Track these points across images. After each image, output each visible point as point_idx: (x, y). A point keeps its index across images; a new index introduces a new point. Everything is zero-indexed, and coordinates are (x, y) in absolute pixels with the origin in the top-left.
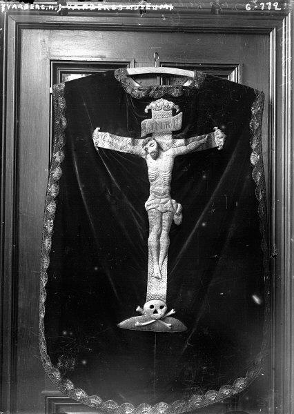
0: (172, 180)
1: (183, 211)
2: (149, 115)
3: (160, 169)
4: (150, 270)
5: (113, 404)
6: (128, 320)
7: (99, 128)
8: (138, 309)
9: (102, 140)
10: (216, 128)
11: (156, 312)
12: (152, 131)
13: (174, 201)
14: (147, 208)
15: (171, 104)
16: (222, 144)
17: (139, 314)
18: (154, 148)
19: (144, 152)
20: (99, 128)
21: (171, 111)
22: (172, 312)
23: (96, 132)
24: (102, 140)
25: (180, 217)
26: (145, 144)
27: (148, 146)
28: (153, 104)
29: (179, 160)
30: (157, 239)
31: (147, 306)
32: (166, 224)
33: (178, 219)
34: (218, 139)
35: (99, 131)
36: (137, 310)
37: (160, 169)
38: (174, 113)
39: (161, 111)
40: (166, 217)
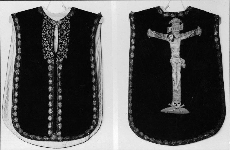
0: (93, 116)
1: (186, 63)
2: (171, 25)
3: (175, 47)
4: (174, 88)
5: (159, 141)
6: (165, 109)
7: (150, 29)
8: (169, 104)
9: (151, 34)
10: (198, 27)
11: (176, 105)
12: (171, 31)
13: (182, 59)
14: (171, 62)
15: (180, 21)
16: (201, 33)
17: (170, 106)
18: (172, 38)
19: (168, 39)
20: (150, 29)
21: (179, 23)
22: (183, 105)
23: (149, 30)
24: (151, 34)
25: (185, 64)
26: (168, 36)
27: (170, 37)
28: (172, 21)
29: (183, 42)
30: (177, 76)
31: (173, 103)
32: (179, 69)
33: (184, 66)
34: (199, 31)
35: (150, 30)
36: (169, 105)
37: (175, 47)
38: (180, 24)
39: (176, 26)
40: (179, 64)
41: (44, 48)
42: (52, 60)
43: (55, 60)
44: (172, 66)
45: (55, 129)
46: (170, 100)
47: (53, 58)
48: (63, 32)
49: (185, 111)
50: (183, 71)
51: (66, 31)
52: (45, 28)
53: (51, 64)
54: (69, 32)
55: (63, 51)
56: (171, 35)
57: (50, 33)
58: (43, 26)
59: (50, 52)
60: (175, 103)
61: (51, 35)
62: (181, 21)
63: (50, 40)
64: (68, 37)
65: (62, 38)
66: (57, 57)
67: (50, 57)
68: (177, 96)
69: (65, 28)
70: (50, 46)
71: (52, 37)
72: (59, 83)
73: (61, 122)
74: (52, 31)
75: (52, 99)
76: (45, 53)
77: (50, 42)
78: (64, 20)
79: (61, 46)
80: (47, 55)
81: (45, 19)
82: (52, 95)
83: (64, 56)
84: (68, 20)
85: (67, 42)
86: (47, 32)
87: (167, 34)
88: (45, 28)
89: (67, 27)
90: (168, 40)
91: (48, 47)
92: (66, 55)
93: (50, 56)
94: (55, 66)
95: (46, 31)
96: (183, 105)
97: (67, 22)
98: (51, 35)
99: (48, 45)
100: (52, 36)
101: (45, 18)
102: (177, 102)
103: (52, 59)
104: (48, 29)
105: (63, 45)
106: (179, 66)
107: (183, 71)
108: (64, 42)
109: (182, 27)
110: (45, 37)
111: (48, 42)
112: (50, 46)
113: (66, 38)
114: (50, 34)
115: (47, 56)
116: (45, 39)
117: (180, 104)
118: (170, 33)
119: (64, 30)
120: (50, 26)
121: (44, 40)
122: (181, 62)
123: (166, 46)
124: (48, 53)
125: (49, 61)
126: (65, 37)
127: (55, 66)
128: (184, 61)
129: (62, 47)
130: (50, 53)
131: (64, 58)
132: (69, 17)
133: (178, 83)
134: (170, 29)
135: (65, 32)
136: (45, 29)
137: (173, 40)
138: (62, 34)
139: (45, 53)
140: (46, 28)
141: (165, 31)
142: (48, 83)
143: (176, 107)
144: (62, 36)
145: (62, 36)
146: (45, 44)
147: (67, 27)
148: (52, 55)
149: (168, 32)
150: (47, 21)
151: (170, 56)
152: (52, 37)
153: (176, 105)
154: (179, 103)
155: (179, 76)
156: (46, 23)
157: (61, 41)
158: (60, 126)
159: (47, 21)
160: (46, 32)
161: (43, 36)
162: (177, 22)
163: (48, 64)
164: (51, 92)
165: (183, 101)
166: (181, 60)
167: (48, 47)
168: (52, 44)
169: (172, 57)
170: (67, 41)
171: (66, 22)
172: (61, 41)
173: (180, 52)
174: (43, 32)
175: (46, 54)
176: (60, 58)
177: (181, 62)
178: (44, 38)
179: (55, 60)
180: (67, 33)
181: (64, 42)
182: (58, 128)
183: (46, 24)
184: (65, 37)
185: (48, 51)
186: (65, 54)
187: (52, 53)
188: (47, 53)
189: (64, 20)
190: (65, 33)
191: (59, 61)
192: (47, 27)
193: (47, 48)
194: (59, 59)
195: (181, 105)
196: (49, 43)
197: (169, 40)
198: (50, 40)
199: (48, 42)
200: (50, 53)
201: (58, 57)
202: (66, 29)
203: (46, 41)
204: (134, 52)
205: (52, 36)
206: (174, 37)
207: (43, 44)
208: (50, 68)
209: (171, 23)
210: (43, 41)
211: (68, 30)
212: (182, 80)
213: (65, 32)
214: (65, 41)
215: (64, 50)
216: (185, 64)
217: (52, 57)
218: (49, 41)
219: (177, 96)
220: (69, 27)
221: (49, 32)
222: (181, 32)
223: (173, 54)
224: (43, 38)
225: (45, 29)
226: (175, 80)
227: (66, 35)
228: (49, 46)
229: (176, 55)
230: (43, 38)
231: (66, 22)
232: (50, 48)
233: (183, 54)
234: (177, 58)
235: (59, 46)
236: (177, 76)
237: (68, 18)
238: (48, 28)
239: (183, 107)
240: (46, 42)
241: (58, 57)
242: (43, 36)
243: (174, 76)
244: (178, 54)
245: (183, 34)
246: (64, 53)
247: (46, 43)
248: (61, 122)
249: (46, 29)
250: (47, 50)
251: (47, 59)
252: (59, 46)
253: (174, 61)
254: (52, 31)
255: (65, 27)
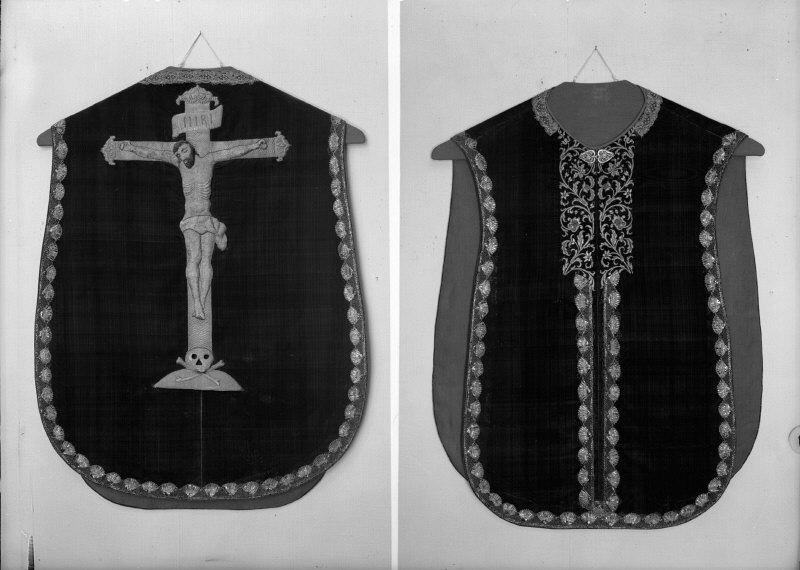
1: (227, 233)
2: (181, 109)
3: (196, 184)
4: (191, 309)
8: (179, 360)
11: (199, 363)
13: (215, 220)
15: (209, 95)
17: (181, 367)
21: (208, 105)
22: (221, 363)
25: (225, 239)
30: (199, 275)
31: (189, 357)
32: (208, 250)
33: (222, 244)
37: (196, 184)
38: (212, 106)
39: (197, 117)
40: (207, 238)
41: (568, 238)
42: (587, 277)
43: (597, 279)
44: (187, 241)
45: (599, 490)
46: (181, 345)
47: (591, 270)
48: (614, 186)
49: (223, 382)
50: (219, 260)
51: (622, 183)
52: (567, 175)
53: (585, 291)
54: (630, 187)
55: (617, 249)
56: (184, 146)
57: (585, 191)
58: (562, 168)
59: (584, 251)
60: (194, 356)
61: (588, 195)
62: (216, 100)
63: (586, 213)
64: (628, 200)
65: (612, 204)
66: (603, 269)
67: (583, 267)
68: (200, 333)
69: (617, 173)
70: (587, 231)
71: (590, 203)
72: (583, 343)
73: (618, 468)
74: (588, 183)
75: (589, 399)
76: (566, 257)
77: (587, 219)
78: (616, 145)
79: (607, 229)
80: (572, 262)
81: (566, 147)
82: (588, 384)
83: (623, 264)
84: (628, 145)
85: (627, 217)
86: (575, 185)
87: (170, 139)
88: (567, 175)
89: (626, 168)
90: (174, 160)
91: (580, 237)
92: (631, 260)
93: (583, 264)
94: (598, 295)
95: (571, 184)
96: (221, 363)
97: (625, 154)
98: (588, 195)
99: (580, 230)
100: (591, 199)
101: (566, 142)
102: (200, 355)
103: (588, 275)
104: (578, 179)
105: (614, 228)
106: (207, 241)
107: (217, 257)
108: (615, 218)
109: (216, 118)
110: (570, 205)
111: (578, 220)
112: (587, 231)
113: (622, 203)
114: (583, 193)
115: (572, 266)
116: (570, 210)
117: (211, 358)
118: (182, 137)
119: (616, 177)
120: (583, 166)
121: (567, 215)
122: (212, 229)
123: (164, 182)
124: (576, 256)
125: (579, 281)
126: (617, 202)
127: (598, 295)
128: (223, 227)
129: (611, 233)
130: (581, 257)
131: (624, 271)
132: (631, 138)
133: (204, 296)
134: (178, 123)
135: (618, 184)
136: (567, 180)
137: (190, 163)
138: (610, 192)
139: (566, 257)
140: (572, 176)
141: (163, 133)
142: (576, 348)
143: (199, 368)
144: (611, 200)
145: (611, 200)
146: (571, 227)
147: (626, 168)
148: (589, 263)
149: (175, 134)
150: (572, 152)
151: (180, 213)
152: (590, 203)
153: (199, 363)
154: (206, 357)
155: (207, 272)
156: (568, 158)
157: (608, 213)
158: (614, 478)
159: (570, 151)
160: (572, 187)
161: (564, 201)
162: (202, 100)
163: (576, 291)
164: (587, 378)
165: (224, 347)
166: (213, 223)
167: (580, 237)
168: (591, 225)
169: (187, 215)
170: (626, 213)
171: (622, 151)
172: (608, 213)
173: (211, 198)
174: (564, 188)
175: (570, 258)
176: (612, 272)
177: (212, 229)
178: (566, 207)
179: (597, 279)
180: (625, 189)
181: (615, 218)
182: (609, 485)
183: (570, 163)
184: (617, 202)
185: (576, 248)
186: (625, 257)
187: (588, 257)
188: (573, 253)
189: (616, 145)
190: (619, 189)
191: (609, 281)
192: (574, 173)
193: (576, 240)
194: (608, 276)
195: (214, 363)
196: (583, 224)
197: (180, 162)
198: (586, 213)
199: (578, 220)
200: (581, 257)
201: (606, 268)
202: (622, 175)
203: (572, 216)
204: (64, 202)
205: (591, 199)
206: (194, 152)
207: (566, 224)
208: (582, 302)
209: (183, 103)
210: (563, 216)
211: (627, 178)
212: (216, 286)
213: (618, 184)
214: (621, 214)
215: (620, 244)
216: (225, 237)
217: (588, 270)
218: (581, 217)
219: (200, 333)
220: (629, 171)
221: (580, 187)
222: (216, 135)
223: (188, 206)
224: (564, 207)
225: (567, 180)
226: (195, 285)
227: (620, 194)
228: (581, 232)
229: (200, 208)
230: (564, 207)
231: (622, 151)
232: (586, 239)
233: (217, 208)
234: (201, 218)
235: (602, 230)
236: (199, 275)
237: (628, 139)
238: (575, 176)
239: (221, 369)
240: (575, 219)
241: (606, 268)
242: (564, 201)
243: (191, 272)
244: (206, 204)
245: (220, 145)
246: (623, 255)
247: (575, 224)
248: (618, 468)
249: (570, 179)
250: (575, 246)
251: (572, 275)
252: (602, 230)
253: (192, 226)
254: (590, 184)
255: (619, 171)
